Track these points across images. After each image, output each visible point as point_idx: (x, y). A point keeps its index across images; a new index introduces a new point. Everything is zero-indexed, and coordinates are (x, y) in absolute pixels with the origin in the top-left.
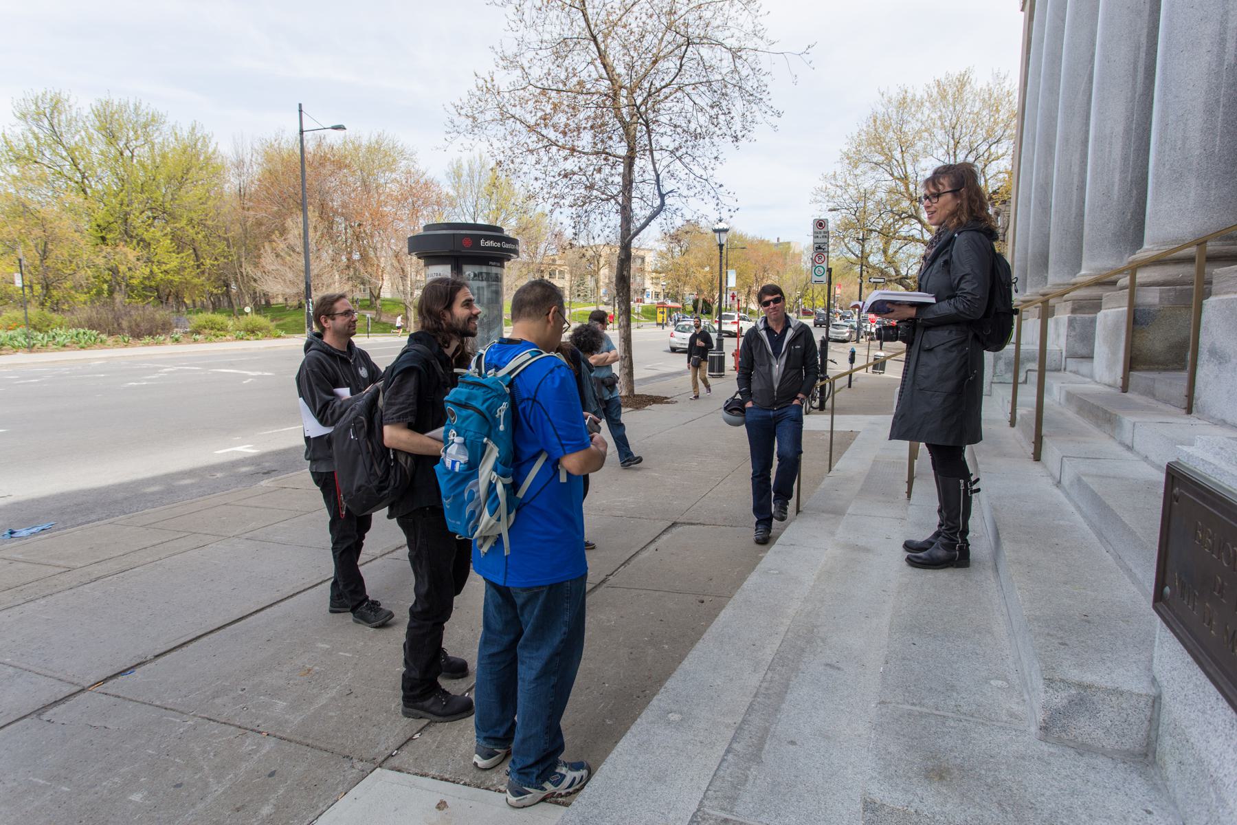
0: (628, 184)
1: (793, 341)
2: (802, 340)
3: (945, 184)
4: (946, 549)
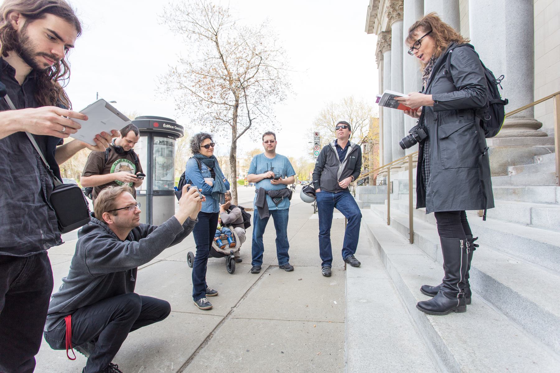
0: (235, 116)
1: (351, 154)
2: (357, 153)
3: (420, 34)
4: (452, 295)
